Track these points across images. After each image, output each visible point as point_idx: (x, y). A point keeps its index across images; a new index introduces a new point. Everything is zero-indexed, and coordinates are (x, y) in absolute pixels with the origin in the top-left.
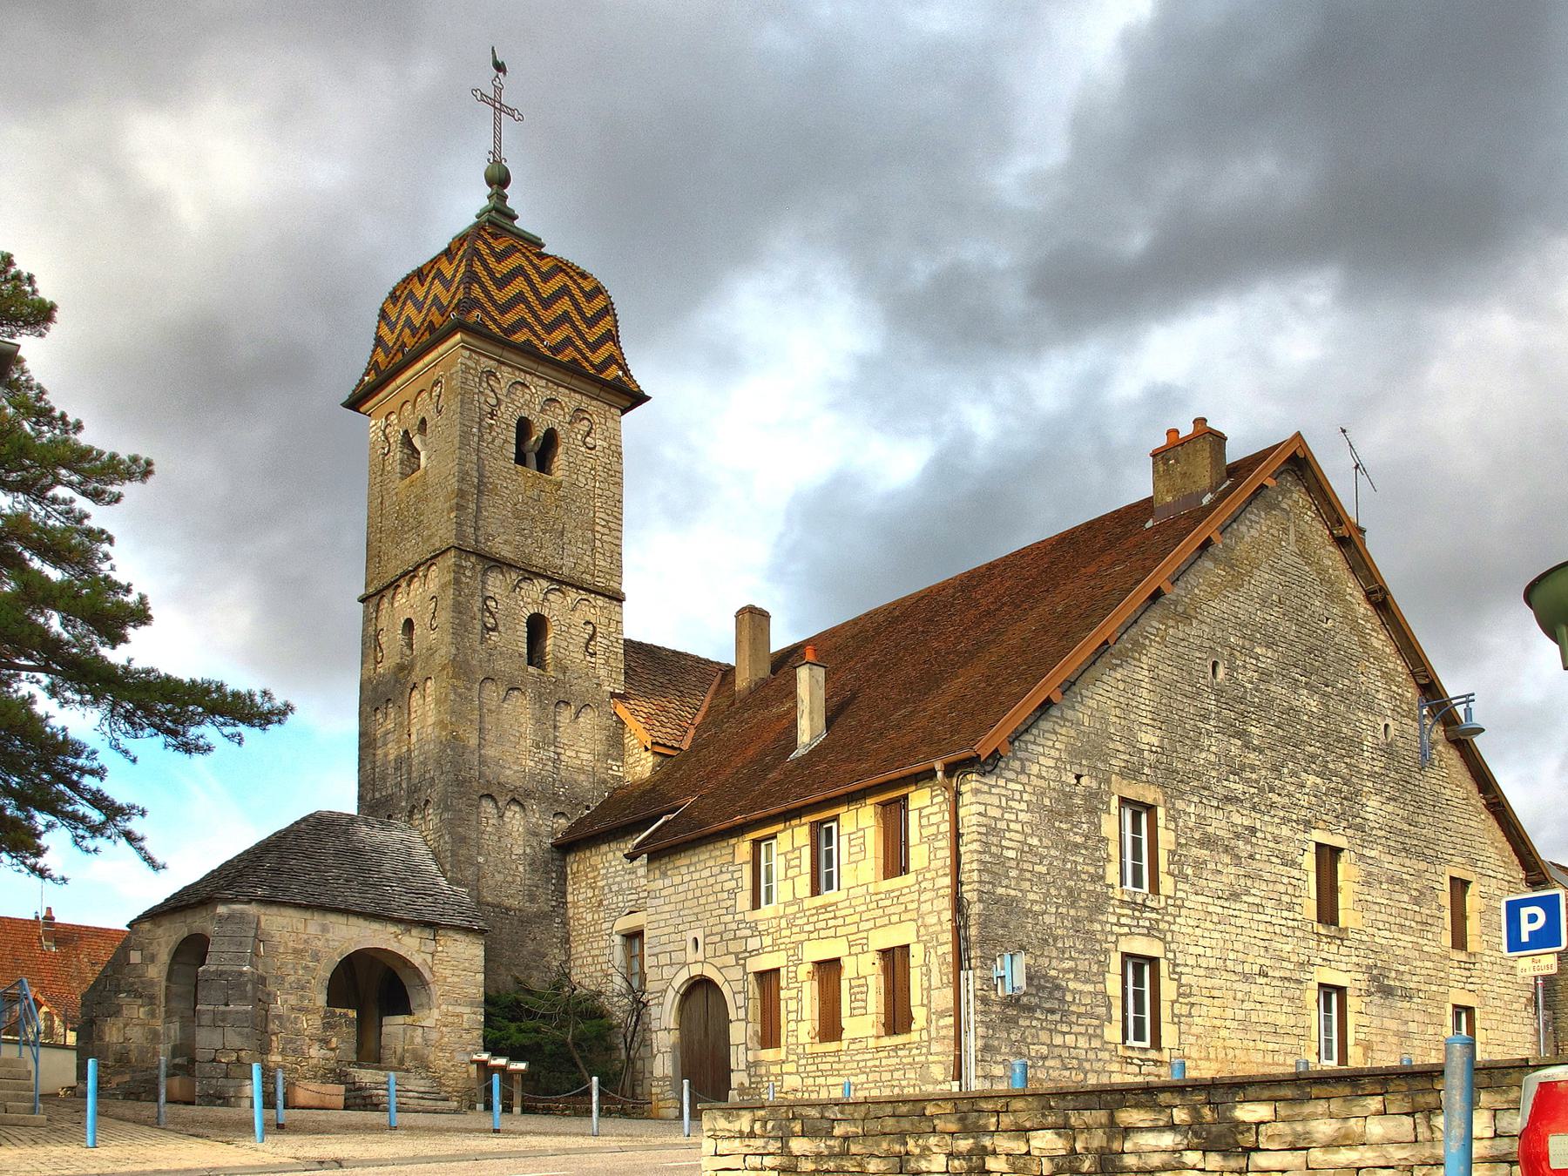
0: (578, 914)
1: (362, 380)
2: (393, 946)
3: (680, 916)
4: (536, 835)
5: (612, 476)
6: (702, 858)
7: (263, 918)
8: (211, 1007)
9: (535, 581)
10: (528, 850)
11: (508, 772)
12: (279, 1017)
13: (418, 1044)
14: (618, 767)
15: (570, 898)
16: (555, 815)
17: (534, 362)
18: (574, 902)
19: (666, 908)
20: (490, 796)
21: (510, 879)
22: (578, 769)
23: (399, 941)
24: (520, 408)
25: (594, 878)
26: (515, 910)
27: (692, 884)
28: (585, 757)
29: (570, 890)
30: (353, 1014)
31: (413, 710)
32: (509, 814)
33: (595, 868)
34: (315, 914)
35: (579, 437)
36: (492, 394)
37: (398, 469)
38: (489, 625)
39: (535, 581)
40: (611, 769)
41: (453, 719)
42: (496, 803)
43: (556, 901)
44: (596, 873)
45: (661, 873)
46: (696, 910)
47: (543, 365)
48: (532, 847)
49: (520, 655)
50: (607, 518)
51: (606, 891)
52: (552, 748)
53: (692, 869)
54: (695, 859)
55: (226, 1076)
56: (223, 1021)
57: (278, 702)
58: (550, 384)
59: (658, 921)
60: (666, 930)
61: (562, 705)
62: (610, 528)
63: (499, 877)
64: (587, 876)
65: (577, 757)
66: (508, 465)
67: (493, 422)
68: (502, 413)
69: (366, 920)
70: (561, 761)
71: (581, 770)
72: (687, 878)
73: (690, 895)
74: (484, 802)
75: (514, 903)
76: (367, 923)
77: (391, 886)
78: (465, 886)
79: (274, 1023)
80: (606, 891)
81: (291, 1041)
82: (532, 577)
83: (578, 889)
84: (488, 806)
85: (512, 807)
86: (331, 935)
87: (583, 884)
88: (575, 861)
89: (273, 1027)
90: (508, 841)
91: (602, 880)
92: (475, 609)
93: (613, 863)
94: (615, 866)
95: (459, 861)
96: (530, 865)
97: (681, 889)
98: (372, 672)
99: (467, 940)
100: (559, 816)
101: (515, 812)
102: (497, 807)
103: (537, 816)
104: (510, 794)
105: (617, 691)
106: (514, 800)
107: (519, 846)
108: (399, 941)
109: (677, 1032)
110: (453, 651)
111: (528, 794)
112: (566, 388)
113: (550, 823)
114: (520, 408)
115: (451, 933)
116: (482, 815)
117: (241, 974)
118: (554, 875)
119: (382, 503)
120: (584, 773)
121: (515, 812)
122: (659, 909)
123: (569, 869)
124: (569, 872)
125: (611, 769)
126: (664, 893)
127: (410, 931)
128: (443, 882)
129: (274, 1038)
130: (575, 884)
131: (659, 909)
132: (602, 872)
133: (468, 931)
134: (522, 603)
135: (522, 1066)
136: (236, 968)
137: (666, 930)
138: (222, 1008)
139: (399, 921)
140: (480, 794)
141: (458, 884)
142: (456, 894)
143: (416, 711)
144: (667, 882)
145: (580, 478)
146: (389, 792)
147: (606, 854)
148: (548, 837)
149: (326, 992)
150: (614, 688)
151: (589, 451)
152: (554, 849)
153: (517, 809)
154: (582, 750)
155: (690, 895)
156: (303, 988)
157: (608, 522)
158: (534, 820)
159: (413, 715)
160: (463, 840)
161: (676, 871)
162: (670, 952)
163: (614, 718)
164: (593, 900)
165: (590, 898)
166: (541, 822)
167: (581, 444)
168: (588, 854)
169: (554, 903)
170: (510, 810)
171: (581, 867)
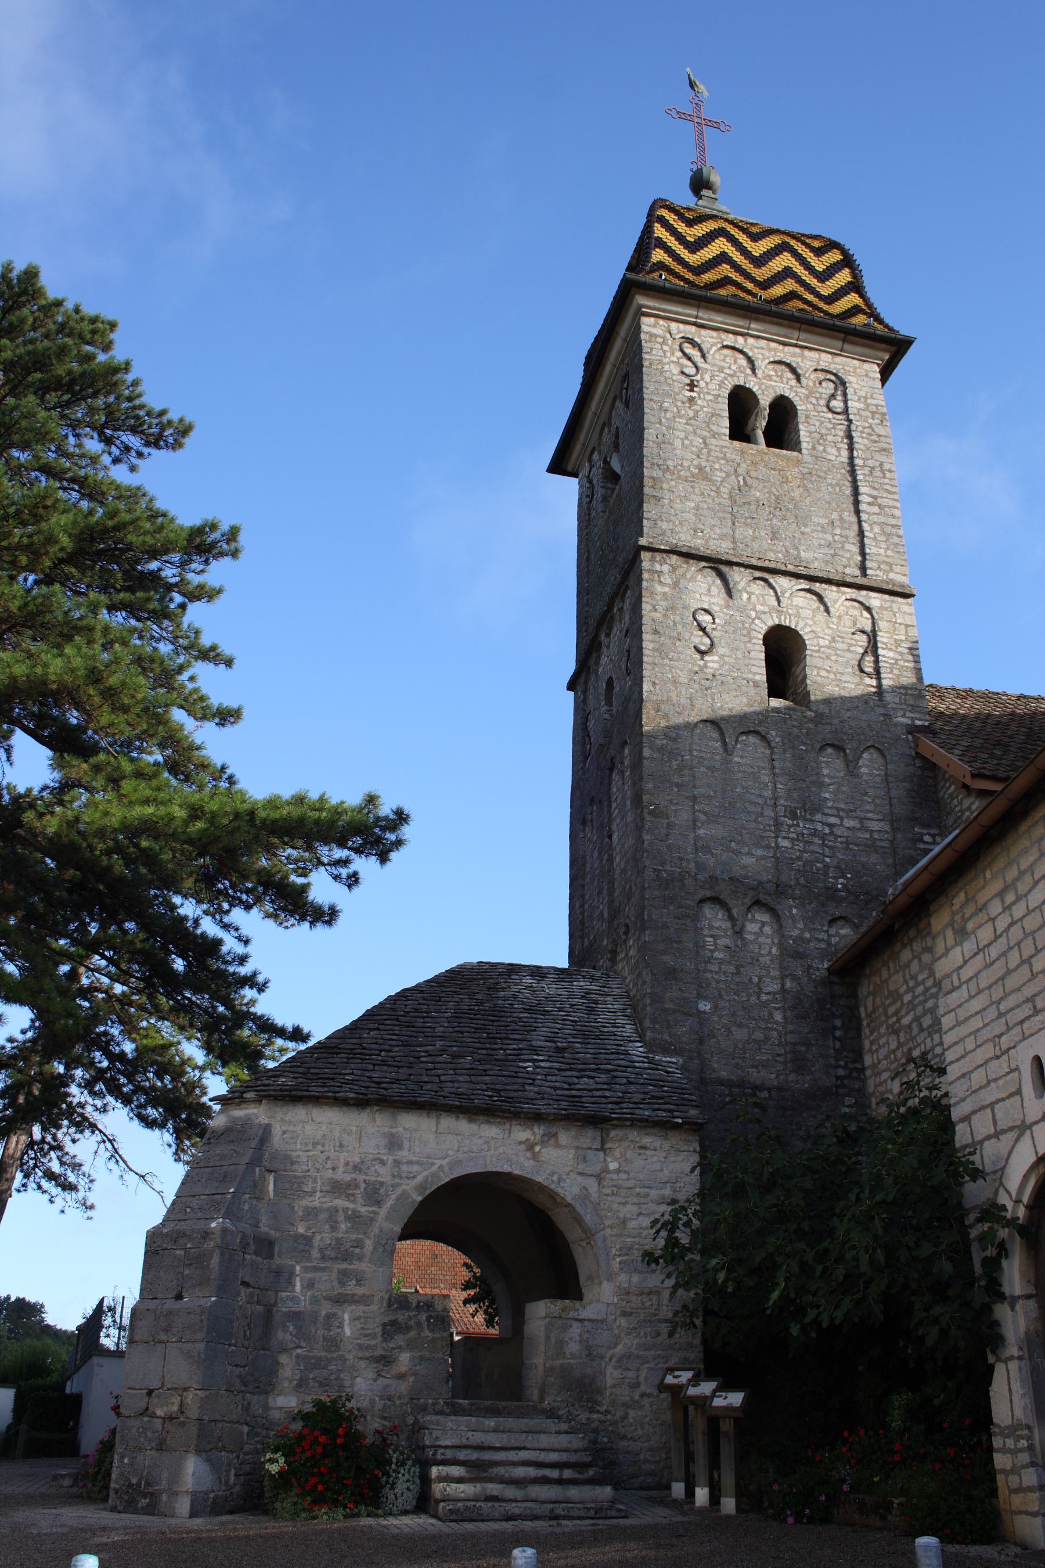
0: (881, 1084)
2: (522, 1166)
3: (1001, 1015)
4: (799, 956)
5: (876, 442)
6: (1024, 863)
7: (277, 1129)
10: (788, 984)
11: (747, 860)
12: (296, 1317)
13: (573, 1356)
15: (868, 1060)
16: (832, 921)
17: (744, 317)
18: (874, 1066)
19: (975, 1005)
20: (715, 900)
21: (759, 1035)
22: (866, 845)
23: (535, 1156)
24: (732, 376)
25: (896, 1013)
26: (770, 1090)
27: (1016, 932)
28: (875, 826)
29: (867, 1044)
32: (752, 927)
33: (896, 996)
34: (377, 1116)
36: (689, 364)
38: (703, 648)
40: (921, 841)
42: (728, 910)
43: (845, 1067)
44: (899, 1004)
45: (956, 932)
46: (1028, 992)
48: (794, 978)
49: (756, 685)
50: (875, 493)
51: (915, 1030)
52: (818, 817)
53: (1010, 898)
54: (1012, 874)
55: (161, 1447)
56: (167, 1330)
57: (386, 809)
59: (962, 1040)
60: (981, 1055)
61: (830, 750)
62: (880, 506)
63: (739, 1034)
64: (886, 1014)
65: (863, 828)
66: (721, 443)
67: (694, 394)
68: (707, 384)
69: (471, 1121)
70: (837, 837)
71: (871, 846)
72: (1002, 924)
73: (1014, 958)
74: (708, 910)
75: (770, 1077)
76: (474, 1127)
77: (534, 1061)
78: (676, 1053)
80: (915, 1030)
81: (319, 1364)
83: (877, 1040)
84: (714, 918)
85: (758, 916)
86: (405, 1153)
87: (883, 1030)
89: (284, 1335)
90: (753, 974)
91: (907, 1013)
93: (920, 978)
94: (923, 981)
95: (665, 1011)
96: (793, 1008)
97: (994, 951)
99: (666, 1145)
100: (840, 923)
101: (763, 924)
102: (731, 918)
103: (800, 925)
104: (751, 894)
105: (918, 723)
106: (757, 903)
107: (773, 978)
108: (535, 1156)
109: (1032, 1304)
111: (781, 890)
112: (796, 346)
113: (823, 936)
114: (732, 376)
115: (633, 1134)
116: (706, 932)
117: (206, 1234)
118: (838, 1023)
120: (876, 852)
122: (962, 1014)
123: (862, 1010)
124: (863, 1014)
125: (921, 841)
126: (967, 973)
127: (555, 1135)
128: (637, 1049)
129: (283, 1359)
130: (872, 1032)
131: (962, 1014)
132: (907, 998)
133: (665, 1126)
134: (753, 614)
135: (736, 1399)
136: (201, 1225)
137: (981, 1055)
138: (171, 1304)
139: (537, 1118)
140: (699, 896)
141: (666, 1051)
142: (655, 1065)
144: (969, 946)
145: (829, 449)
147: (908, 965)
148: (822, 959)
150: (913, 719)
152: (834, 979)
153: (766, 918)
154: (870, 815)
155: (1014, 958)
156: (347, 1257)
157: (875, 497)
158: (795, 933)
159: (614, 805)
160: (672, 974)
161: (982, 917)
162: (991, 1106)
163: (918, 763)
164: (899, 1054)
165: (894, 1051)
166: (807, 935)
167: (825, 409)
168: (885, 974)
169: (841, 1072)
170: (753, 920)
171: (878, 1001)
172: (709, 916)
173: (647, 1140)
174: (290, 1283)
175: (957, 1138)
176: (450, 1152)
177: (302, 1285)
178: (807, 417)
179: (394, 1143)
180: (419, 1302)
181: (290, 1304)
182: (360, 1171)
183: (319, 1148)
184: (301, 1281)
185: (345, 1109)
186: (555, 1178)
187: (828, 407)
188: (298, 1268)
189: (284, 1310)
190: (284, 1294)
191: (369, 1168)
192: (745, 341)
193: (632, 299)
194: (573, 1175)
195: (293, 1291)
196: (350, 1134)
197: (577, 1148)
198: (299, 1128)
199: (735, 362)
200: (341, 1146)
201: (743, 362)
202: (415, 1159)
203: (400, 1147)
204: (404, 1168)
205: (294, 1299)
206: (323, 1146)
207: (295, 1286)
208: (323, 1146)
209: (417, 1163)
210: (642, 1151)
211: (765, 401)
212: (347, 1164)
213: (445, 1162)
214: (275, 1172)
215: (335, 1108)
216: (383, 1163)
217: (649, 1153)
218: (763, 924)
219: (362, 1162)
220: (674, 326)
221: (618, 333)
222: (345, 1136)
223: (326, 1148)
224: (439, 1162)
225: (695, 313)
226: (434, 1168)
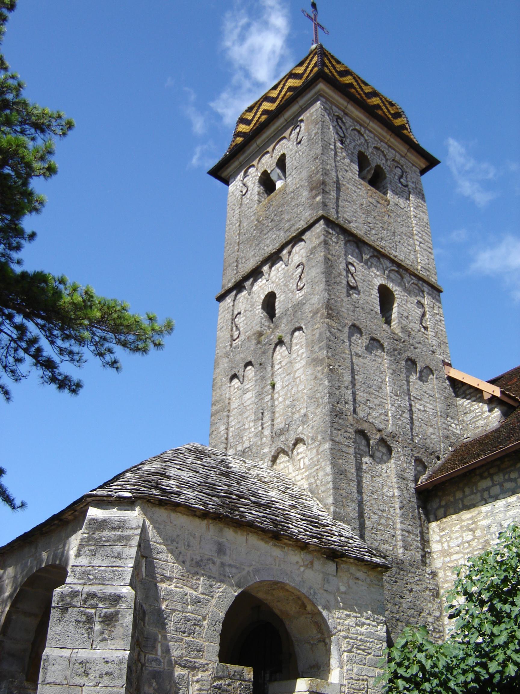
1: (231, 145)
8: (66, 653)
9: (381, 260)
14: (456, 425)
30: (248, 673)
31: (276, 362)
34: (211, 526)
35: (397, 177)
37: (256, 198)
39: (381, 260)
41: (330, 354)
47: (373, 122)
58: (376, 138)
79: (150, 685)
82: (379, 256)
88: (440, 507)
92: (341, 267)
98: (229, 347)
110: (326, 295)
119: (239, 226)
121: (383, 453)
143: (280, 363)
146: (246, 445)
149: (218, 639)
151: (403, 188)
159: (277, 367)
164: (474, 543)
172: (358, 442)
173: (359, 574)
174: (154, 647)
175: (133, 562)
176: (254, 563)
177: (162, 650)
178: (391, 182)
179: (221, 550)
180: (235, 672)
181: (154, 664)
182: (200, 566)
183: (175, 543)
184: (162, 646)
185: (191, 518)
186: (312, 591)
187: (400, 181)
188: (160, 636)
189: (150, 669)
190: (150, 656)
191: (205, 566)
192: (365, 131)
193: (316, 85)
194: (321, 591)
195: (156, 654)
196: (194, 537)
197: (323, 572)
198: (163, 526)
199: (360, 139)
200: (189, 545)
201: (238, 315)
202: (233, 563)
203: (225, 554)
204: (227, 569)
205: (156, 660)
206: (177, 543)
207: (157, 651)
208: (177, 543)
209: (235, 567)
210: (357, 581)
211: (373, 165)
212: (192, 560)
213: (251, 569)
214: (147, 558)
215: (185, 516)
216: (214, 563)
217: (360, 583)
218: (383, 453)
219: (202, 560)
220: (334, 108)
221: (297, 102)
222: (191, 538)
223: (179, 545)
224: (247, 569)
225: (345, 104)
226: (244, 573)
